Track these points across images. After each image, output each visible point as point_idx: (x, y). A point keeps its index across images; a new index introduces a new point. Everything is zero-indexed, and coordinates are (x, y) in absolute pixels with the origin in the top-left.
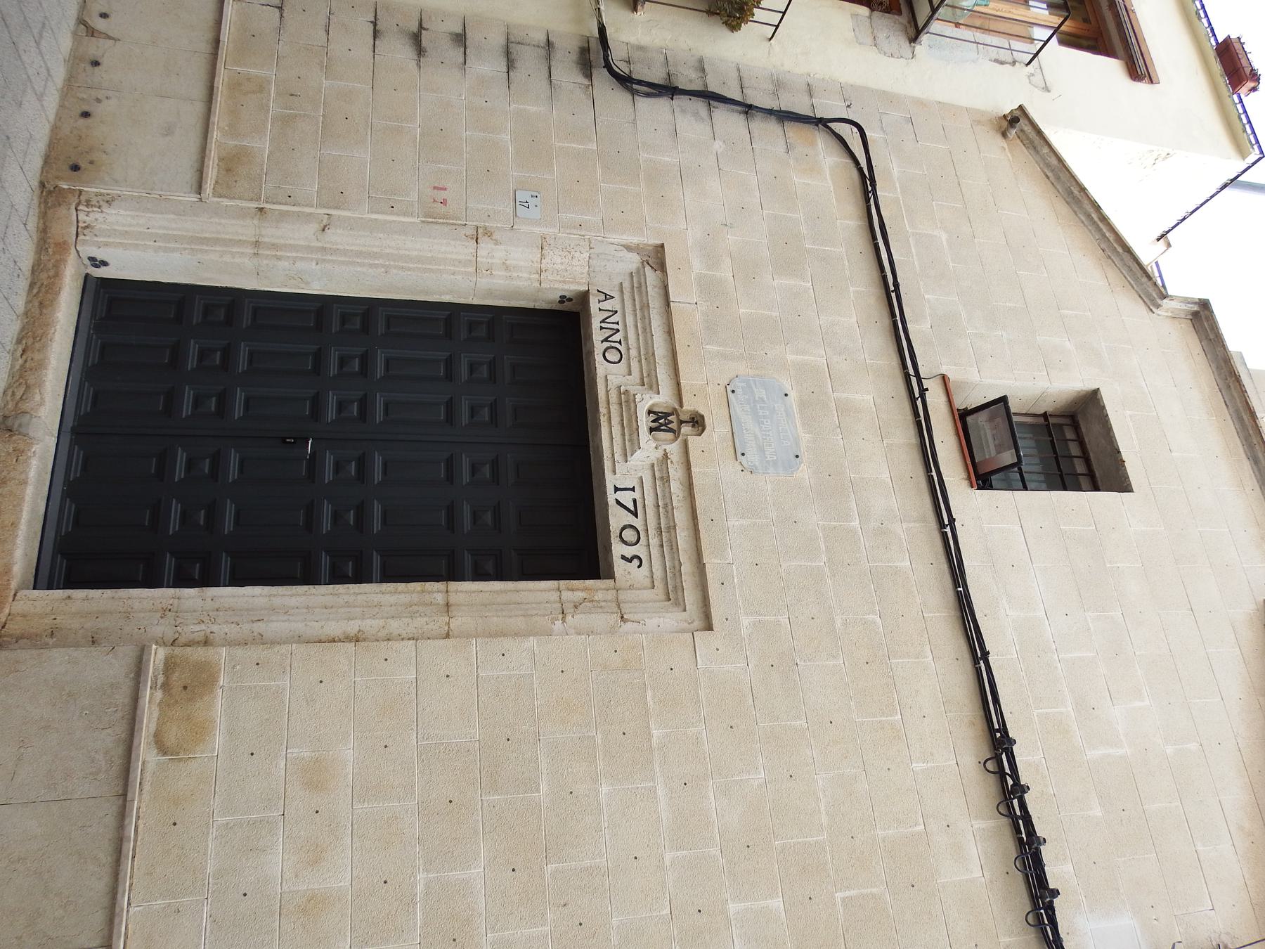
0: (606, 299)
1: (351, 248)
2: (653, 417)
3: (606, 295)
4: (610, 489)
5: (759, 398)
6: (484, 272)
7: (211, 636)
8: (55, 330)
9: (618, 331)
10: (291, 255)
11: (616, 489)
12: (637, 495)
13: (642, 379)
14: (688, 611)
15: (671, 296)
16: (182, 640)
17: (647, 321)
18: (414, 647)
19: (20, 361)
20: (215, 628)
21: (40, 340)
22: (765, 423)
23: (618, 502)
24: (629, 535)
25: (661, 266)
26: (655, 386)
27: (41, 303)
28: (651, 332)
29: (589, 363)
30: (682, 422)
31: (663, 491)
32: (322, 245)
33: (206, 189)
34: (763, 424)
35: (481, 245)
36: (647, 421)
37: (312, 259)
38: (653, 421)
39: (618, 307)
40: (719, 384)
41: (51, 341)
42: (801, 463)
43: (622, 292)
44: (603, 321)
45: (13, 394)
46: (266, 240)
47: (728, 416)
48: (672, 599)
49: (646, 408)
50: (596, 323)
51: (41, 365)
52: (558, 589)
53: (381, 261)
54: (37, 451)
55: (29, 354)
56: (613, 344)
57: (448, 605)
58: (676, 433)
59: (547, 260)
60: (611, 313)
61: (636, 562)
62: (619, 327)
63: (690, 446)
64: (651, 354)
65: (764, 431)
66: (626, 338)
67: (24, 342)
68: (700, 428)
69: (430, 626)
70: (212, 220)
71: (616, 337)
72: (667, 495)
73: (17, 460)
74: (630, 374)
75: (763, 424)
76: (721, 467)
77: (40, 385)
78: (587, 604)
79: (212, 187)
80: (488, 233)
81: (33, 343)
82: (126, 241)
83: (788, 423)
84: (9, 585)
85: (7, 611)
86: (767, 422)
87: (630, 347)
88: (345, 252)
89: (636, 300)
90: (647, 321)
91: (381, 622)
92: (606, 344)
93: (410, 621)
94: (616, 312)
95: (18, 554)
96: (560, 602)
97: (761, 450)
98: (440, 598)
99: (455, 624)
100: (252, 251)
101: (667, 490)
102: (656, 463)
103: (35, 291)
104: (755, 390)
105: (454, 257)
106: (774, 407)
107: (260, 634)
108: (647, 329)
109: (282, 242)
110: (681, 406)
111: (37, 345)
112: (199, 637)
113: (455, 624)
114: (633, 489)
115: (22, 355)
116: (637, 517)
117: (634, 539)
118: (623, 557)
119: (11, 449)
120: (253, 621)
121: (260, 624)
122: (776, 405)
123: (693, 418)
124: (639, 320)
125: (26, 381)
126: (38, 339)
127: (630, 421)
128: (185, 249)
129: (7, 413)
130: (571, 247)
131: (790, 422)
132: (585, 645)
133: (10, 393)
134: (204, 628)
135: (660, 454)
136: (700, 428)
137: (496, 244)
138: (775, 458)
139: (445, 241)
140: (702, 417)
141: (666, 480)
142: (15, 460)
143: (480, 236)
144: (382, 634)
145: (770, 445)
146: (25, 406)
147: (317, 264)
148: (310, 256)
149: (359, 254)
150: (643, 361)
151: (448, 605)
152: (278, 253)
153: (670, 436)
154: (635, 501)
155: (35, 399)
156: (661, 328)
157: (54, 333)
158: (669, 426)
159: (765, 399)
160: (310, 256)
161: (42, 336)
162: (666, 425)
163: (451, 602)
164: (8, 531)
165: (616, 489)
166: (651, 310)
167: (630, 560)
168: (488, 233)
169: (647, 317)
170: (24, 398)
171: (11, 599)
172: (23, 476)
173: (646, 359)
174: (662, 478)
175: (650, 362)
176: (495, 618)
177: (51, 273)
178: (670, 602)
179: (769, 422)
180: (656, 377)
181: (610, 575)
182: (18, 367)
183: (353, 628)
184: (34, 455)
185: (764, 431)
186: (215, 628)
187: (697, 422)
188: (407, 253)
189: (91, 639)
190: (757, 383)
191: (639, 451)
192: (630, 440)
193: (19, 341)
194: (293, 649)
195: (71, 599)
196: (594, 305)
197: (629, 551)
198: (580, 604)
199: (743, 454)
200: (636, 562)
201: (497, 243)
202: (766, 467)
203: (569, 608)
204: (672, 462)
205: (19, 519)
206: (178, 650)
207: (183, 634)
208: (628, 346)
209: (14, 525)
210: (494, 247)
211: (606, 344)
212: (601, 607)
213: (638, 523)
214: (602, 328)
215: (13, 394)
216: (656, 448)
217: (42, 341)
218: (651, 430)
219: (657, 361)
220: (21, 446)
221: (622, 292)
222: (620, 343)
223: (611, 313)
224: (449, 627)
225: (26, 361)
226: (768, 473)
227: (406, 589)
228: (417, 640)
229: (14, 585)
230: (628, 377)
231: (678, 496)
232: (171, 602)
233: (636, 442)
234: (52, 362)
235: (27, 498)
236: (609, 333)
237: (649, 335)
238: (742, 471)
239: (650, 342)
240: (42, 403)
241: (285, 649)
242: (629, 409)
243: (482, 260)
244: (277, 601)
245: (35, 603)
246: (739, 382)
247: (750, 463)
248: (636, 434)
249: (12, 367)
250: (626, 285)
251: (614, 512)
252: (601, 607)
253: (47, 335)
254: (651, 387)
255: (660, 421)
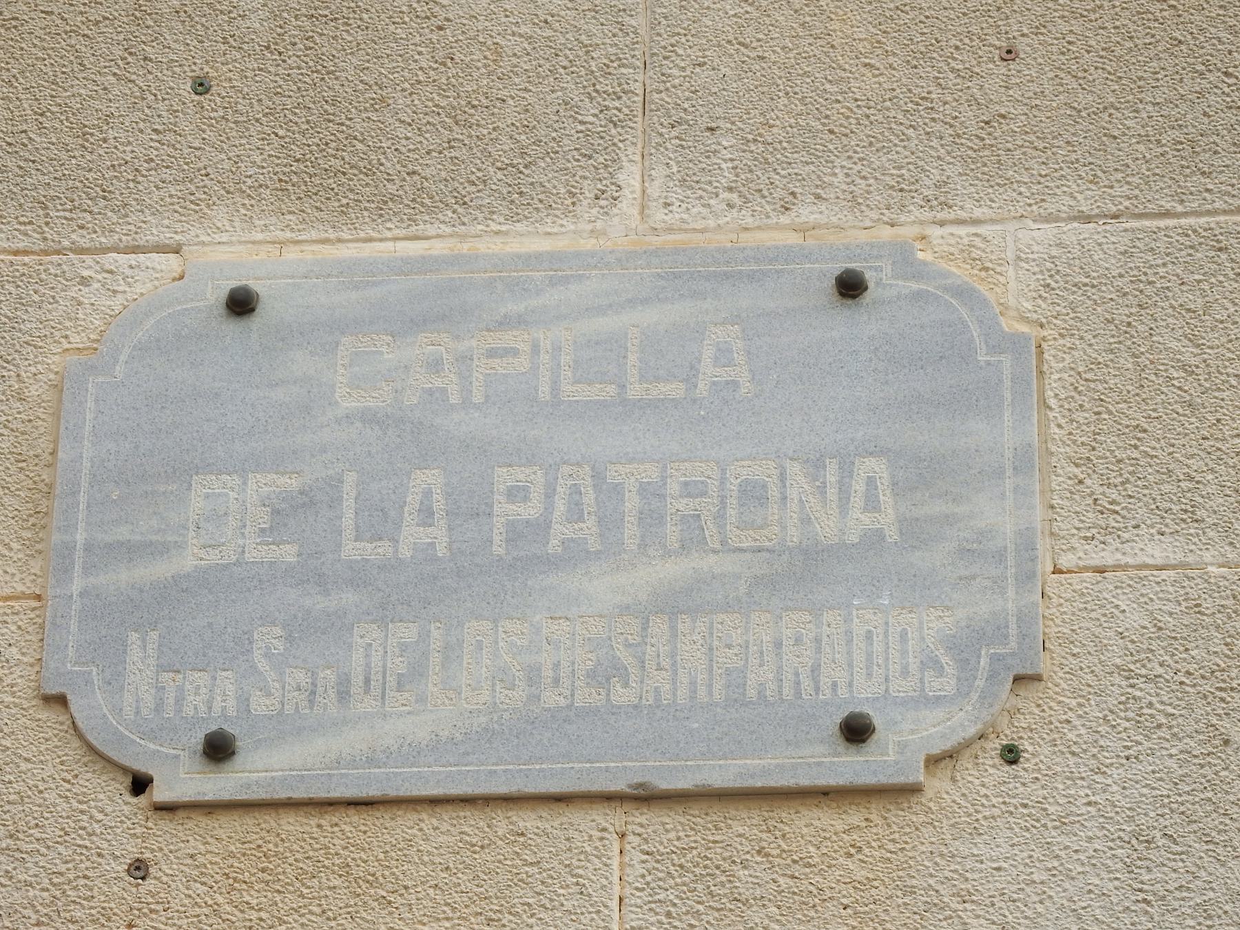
5: (273, 532)
22: (530, 510)
34: (542, 526)
40: (139, 869)
42: (903, 257)
47: (472, 823)
75: (542, 526)
83: (505, 323)
86: (516, 494)
104: (187, 561)
106: (369, 418)
122: (348, 404)
131: (513, 307)
138: (876, 467)
145: (753, 494)
159: (292, 483)
179: (520, 474)
190: (123, 533)
202: (964, 552)
226: (1027, 545)
238: (1011, 755)
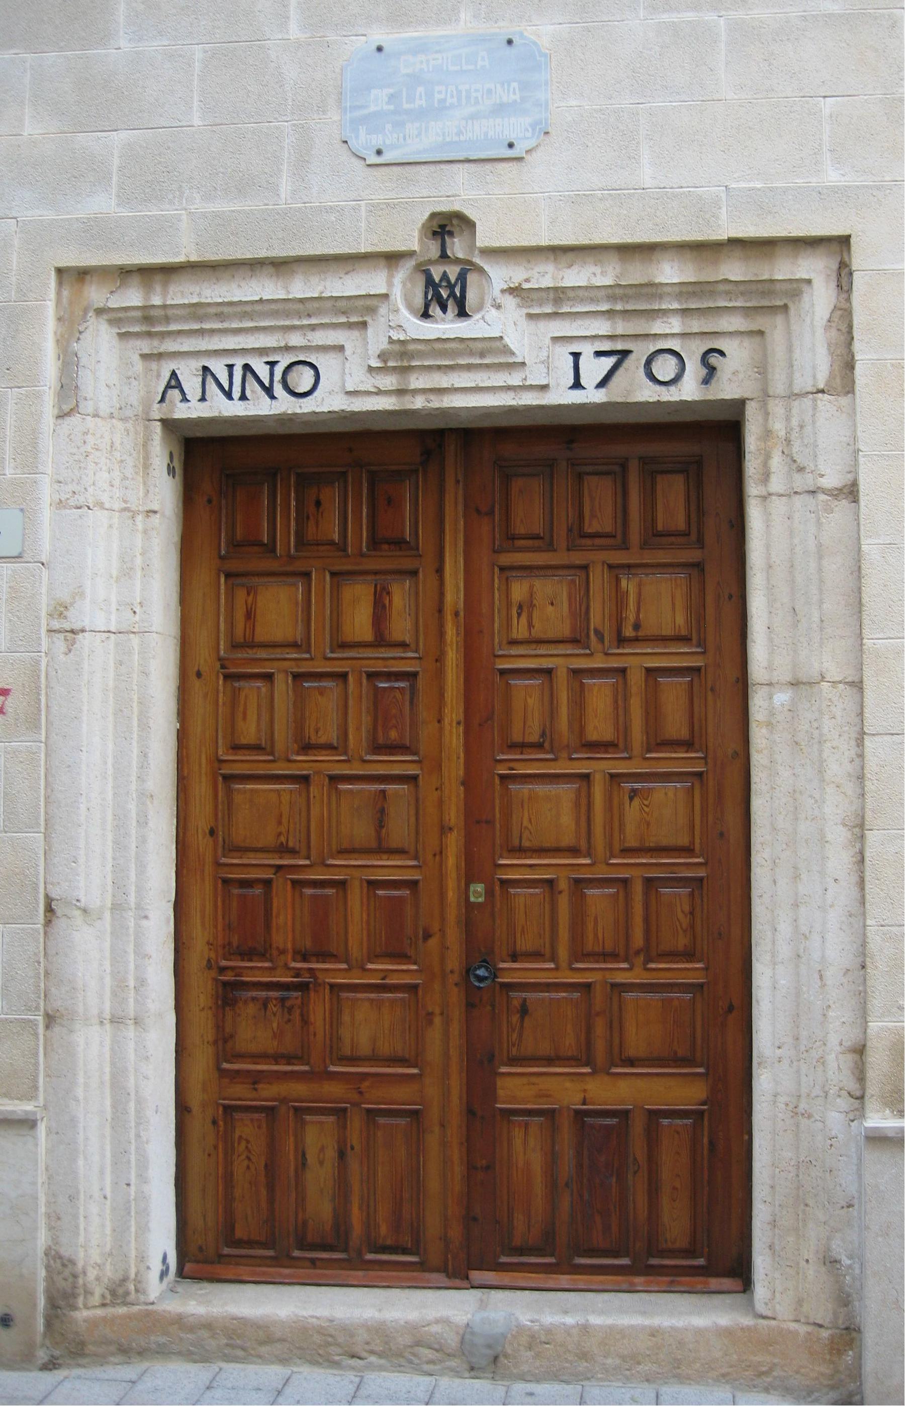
0: (179, 386)
1: (110, 860)
2: (435, 310)
3: (168, 387)
4: (577, 397)
6: (137, 618)
7: (847, 1044)
8: (312, 1317)
9: (247, 367)
10: (132, 962)
11: (577, 385)
12: (587, 350)
13: (350, 326)
14: (811, 276)
15: (177, 260)
16: (852, 1085)
17: (226, 310)
18: (876, 738)
19: (373, 1359)
20: (833, 1040)
21: (331, 1336)
22: (442, 96)
23: (602, 384)
24: (665, 368)
25: (82, 274)
26: (369, 302)
27: (262, 1343)
28: (253, 302)
29: (306, 423)
30: (444, 256)
31: (582, 300)
32: (109, 912)
33: (25, 1111)
35: (87, 624)
36: (443, 320)
37: (138, 926)
38: (444, 308)
39: (196, 364)
41: (331, 1321)
43: (160, 356)
44: (229, 395)
45: (431, 1362)
46: (107, 1006)
47: (432, 168)
48: (785, 301)
49: (418, 322)
50: (234, 409)
51: (379, 1330)
52: (765, 498)
53: (132, 807)
54: (528, 1317)
55: (358, 1349)
56: (278, 376)
57: (795, 684)
58: (467, 268)
59: (105, 498)
60: (209, 379)
61: (714, 360)
62: (239, 363)
63: (496, 244)
64: (301, 306)
65: (459, 99)
66: (261, 351)
67: (337, 1358)
68: (455, 222)
69: (839, 714)
70: (81, 1098)
71: (263, 372)
72: (592, 294)
73: (547, 1343)
74: (341, 348)
76: (537, 189)
77: (412, 1328)
78: (794, 450)
79: (16, 1102)
80: (60, 610)
81: (339, 1345)
82: (133, 1229)
84: (749, 1328)
85: (793, 1326)
87: (282, 344)
88: (119, 871)
89: (180, 328)
90: (226, 310)
91: (830, 789)
92: (278, 390)
93: (828, 744)
94: (205, 369)
95: (700, 1321)
96: (789, 496)
97: (500, 109)
98: (782, 698)
99: (834, 673)
100: (132, 1027)
101: (581, 293)
102: (525, 311)
103: (240, 1353)
104: (373, 108)
105: (112, 675)
107: (844, 975)
108: (223, 311)
109: (108, 980)
110: (411, 254)
111: (341, 1340)
112: (849, 1060)
113: (834, 673)
114: (576, 356)
115: (360, 1358)
116: (630, 352)
117: (672, 361)
118: (706, 381)
119: (529, 1353)
120: (824, 986)
121: (828, 974)
123: (435, 233)
124: (226, 325)
125: (406, 1347)
126: (330, 1339)
127: (444, 353)
128: (138, 1136)
129: (466, 1366)
130: (75, 450)
132: (876, 458)
133: (426, 1367)
134: (833, 1055)
135: (510, 302)
136: (455, 222)
137: (82, 595)
139: (85, 691)
140: (433, 215)
141: (559, 294)
142: (548, 1346)
143: (67, 626)
144: (850, 788)
146: (452, 1341)
147: (146, 917)
148: (131, 931)
149: (119, 845)
150: (314, 321)
151: (795, 684)
152: (132, 983)
153: (471, 278)
154: (599, 354)
155: (440, 1331)
156: (243, 284)
157: (318, 1318)
158: (453, 281)
160: (131, 931)
161: (325, 1335)
162: (451, 287)
163: (788, 677)
164: (663, 1339)
165: (577, 385)
166: (203, 300)
167: (712, 370)
168: (60, 610)
169: (219, 309)
170: (436, 1346)
171: (773, 1323)
172: (575, 1332)
173: (309, 316)
174: (557, 301)
175: (318, 309)
176: (825, 606)
177: (205, 1334)
178: (790, 305)
180: (349, 298)
181: (740, 405)
182: (382, 1361)
183: (838, 835)
184: (537, 1321)
185: (459, 99)
186: (833, 1040)
187: (442, 227)
188: (110, 761)
189: (845, 1210)
191: (507, 340)
192: (482, 355)
193: (336, 1365)
194: (875, 923)
195: (773, 1243)
196: (182, 412)
197: (693, 370)
198: (795, 461)
199: (511, 145)
200: (714, 360)
201: (79, 593)
203: (801, 482)
204: (527, 280)
205: (644, 1328)
206: (872, 1089)
207: (841, 1085)
208: (280, 348)
209: (654, 1332)
210: (88, 600)
211: (278, 390)
212: (801, 427)
213: (641, 351)
214: (243, 397)
215: (431, 1362)
216: (498, 307)
217: (334, 1333)
218: (463, 313)
219: (316, 295)
220: (524, 1340)
221: (160, 356)
222: (272, 364)
223: (209, 379)
224: (840, 682)
225: (372, 1352)
227: (765, 752)
228: (865, 733)
229: (747, 1321)
230: (348, 352)
231: (594, 274)
232: (783, 1106)
233: (487, 345)
234: (371, 1315)
235: (609, 1321)
236: (251, 384)
237: (258, 307)
239: (273, 306)
240: (446, 1321)
241: (871, 931)
242: (420, 354)
243: (113, 622)
244: (784, 950)
245: (779, 1289)
246: (357, 137)
247: (529, 134)
248: (472, 345)
249: (381, 1368)
250: (145, 346)
251: (614, 393)
252: (801, 427)
253: (322, 1327)
254: (372, 310)
255: (445, 296)
